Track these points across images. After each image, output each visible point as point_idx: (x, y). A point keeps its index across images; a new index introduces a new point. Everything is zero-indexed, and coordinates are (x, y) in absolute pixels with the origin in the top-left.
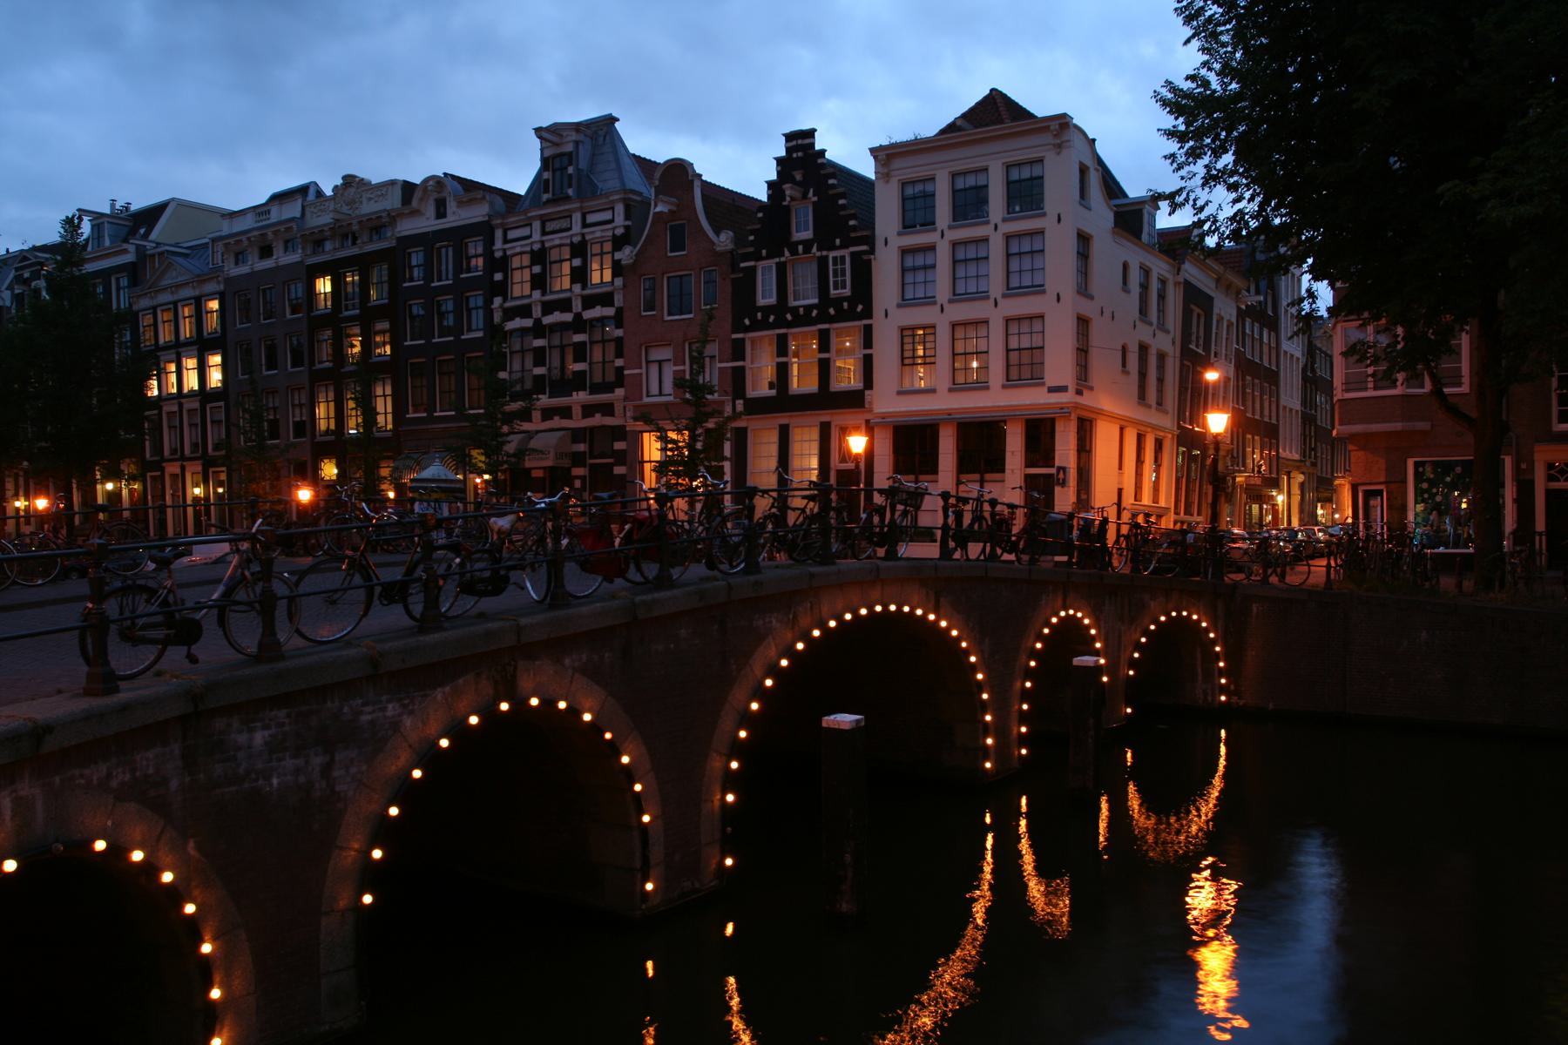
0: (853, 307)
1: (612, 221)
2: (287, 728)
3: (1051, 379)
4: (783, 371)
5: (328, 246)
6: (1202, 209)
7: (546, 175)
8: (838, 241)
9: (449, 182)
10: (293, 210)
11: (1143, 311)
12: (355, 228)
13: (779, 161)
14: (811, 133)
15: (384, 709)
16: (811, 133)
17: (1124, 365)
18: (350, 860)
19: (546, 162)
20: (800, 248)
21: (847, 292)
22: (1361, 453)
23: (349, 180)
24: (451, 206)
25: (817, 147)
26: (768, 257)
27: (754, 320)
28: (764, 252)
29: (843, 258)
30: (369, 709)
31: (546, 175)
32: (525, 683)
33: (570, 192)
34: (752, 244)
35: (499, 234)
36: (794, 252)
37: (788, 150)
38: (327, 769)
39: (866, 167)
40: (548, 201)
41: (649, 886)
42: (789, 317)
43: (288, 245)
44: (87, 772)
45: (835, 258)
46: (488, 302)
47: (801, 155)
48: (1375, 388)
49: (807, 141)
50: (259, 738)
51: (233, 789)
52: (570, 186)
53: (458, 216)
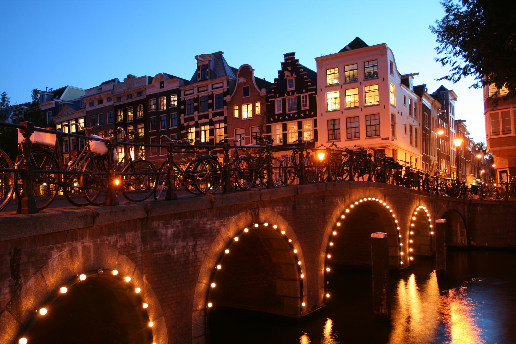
0: (310, 113)
1: (222, 87)
2: (180, 228)
3: (383, 136)
4: (285, 136)
5: (122, 99)
6: (453, 64)
7: (199, 72)
8: (304, 91)
9: (165, 76)
10: (110, 87)
11: (411, 114)
12: (132, 93)
13: (282, 64)
14: (293, 54)
15: (214, 223)
16: (293, 54)
17: (405, 132)
18: (202, 288)
19: (198, 67)
20: (291, 93)
21: (308, 108)
22: (497, 158)
23: (129, 76)
24: (165, 84)
25: (296, 58)
26: (279, 97)
27: (274, 119)
28: (278, 95)
29: (306, 96)
30: (209, 223)
31: (199, 72)
32: (262, 217)
33: (208, 77)
34: (273, 92)
35: (182, 93)
36: (288, 95)
37: (285, 60)
38: (194, 247)
39: (313, 67)
40: (200, 81)
41: (304, 304)
42: (287, 117)
43: (109, 99)
44: (109, 238)
45: (303, 97)
46: (179, 116)
47: (290, 62)
48: (503, 134)
49: (292, 57)
50: (170, 231)
51: (160, 253)
52: (208, 75)
53: (168, 87)
